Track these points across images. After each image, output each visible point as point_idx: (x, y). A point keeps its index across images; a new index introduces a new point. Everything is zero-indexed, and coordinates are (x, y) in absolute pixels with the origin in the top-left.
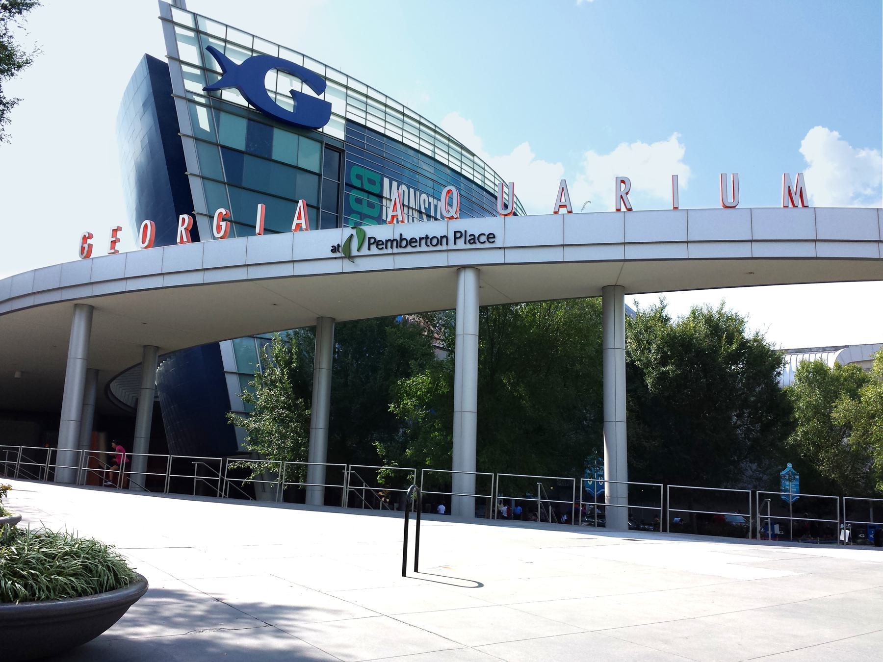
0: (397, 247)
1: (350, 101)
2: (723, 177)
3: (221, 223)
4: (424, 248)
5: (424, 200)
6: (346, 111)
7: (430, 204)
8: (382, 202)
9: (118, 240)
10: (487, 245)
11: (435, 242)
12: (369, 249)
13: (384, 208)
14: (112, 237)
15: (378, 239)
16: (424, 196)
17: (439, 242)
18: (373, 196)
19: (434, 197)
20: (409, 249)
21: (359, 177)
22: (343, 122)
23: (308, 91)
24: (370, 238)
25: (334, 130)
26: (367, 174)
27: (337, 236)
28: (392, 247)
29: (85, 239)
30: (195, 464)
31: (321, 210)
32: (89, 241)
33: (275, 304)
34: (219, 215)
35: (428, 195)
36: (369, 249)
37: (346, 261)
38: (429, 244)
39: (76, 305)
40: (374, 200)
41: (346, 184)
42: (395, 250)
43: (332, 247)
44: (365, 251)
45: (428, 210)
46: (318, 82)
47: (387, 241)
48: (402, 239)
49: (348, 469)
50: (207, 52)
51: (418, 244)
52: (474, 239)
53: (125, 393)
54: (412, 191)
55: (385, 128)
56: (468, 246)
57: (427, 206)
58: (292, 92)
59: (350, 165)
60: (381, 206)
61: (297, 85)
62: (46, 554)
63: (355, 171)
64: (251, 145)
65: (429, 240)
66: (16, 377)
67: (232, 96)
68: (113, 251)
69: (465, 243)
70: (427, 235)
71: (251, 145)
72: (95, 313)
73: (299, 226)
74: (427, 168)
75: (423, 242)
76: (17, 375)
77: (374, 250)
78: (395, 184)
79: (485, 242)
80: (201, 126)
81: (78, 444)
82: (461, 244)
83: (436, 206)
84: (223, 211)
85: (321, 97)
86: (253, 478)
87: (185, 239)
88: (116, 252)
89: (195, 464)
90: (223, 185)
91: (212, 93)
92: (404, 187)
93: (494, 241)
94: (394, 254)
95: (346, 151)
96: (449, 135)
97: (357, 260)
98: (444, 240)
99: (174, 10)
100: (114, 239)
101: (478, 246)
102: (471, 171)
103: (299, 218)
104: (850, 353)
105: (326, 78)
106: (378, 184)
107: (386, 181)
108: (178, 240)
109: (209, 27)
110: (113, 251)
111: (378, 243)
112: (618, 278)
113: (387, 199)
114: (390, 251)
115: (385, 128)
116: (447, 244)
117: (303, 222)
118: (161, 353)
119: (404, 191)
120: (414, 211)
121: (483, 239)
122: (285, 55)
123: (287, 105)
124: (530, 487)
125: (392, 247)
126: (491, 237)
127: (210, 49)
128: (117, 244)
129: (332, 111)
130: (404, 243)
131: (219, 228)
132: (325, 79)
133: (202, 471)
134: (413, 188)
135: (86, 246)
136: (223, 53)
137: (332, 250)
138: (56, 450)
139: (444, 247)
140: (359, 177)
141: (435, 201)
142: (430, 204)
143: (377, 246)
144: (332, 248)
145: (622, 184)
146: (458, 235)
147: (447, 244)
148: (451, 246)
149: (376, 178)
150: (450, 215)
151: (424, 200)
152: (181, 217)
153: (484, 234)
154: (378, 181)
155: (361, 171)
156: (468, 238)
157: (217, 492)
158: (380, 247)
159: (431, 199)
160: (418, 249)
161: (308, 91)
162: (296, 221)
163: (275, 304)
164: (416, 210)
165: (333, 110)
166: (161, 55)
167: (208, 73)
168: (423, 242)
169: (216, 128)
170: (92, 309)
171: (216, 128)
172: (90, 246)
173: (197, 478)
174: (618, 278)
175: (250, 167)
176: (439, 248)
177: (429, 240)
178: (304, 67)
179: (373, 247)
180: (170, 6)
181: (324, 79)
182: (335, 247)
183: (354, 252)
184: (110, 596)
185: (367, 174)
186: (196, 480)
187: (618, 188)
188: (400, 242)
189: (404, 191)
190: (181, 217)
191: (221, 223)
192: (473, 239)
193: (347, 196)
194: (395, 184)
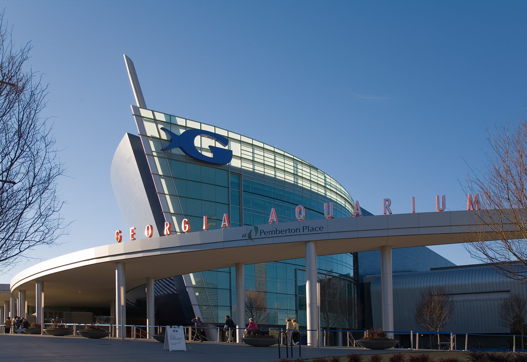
1: (243, 148)
2: (438, 197)
3: (186, 225)
4: (288, 234)
6: (241, 153)
10: (320, 232)
14: (132, 232)
23: (219, 145)
27: (245, 230)
29: (118, 234)
30: (131, 327)
31: (230, 205)
37: (250, 241)
38: (290, 232)
41: (243, 191)
42: (274, 235)
44: (258, 236)
52: (313, 229)
53: (132, 298)
55: (302, 174)
58: (210, 147)
65: (290, 230)
68: (133, 239)
69: (308, 231)
75: (288, 231)
77: (263, 235)
80: (175, 217)
82: (306, 231)
84: (187, 220)
85: (226, 148)
86: (197, 334)
88: (135, 239)
90: (165, 159)
95: (242, 174)
98: (298, 230)
99: (140, 109)
100: (133, 233)
101: (315, 232)
102: (316, 178)
103: (225, 221)
105: (228, 137)
110: (133, 239)
114: (271, 235)
115: (302, 174)
116: (299, 232)
121: (317, 229)
129: (233, 154)
130: (278, 232)
131: (185, 227)
135: (119, 236)
136: (170, 130)
138: (155, 326)
139: (298, 233)
145: (387, 202)
147: (299, 232)
153: (318, 227)
156: (310, 229)
160: (285, 234)
161: (219, 145)
165: (233, 154)
166: (137, 132)
168: (288, 231)
169: (170, 168)
171: (170, 168)
172: (121, 236)
176: (295, 233)
177: (290, 230)
178: (216, 133)
180: (139, 108)
181: (227, 138)
183: (253, 236)
184: (251, 339)
187: (385, 204)
191: (186, 225)
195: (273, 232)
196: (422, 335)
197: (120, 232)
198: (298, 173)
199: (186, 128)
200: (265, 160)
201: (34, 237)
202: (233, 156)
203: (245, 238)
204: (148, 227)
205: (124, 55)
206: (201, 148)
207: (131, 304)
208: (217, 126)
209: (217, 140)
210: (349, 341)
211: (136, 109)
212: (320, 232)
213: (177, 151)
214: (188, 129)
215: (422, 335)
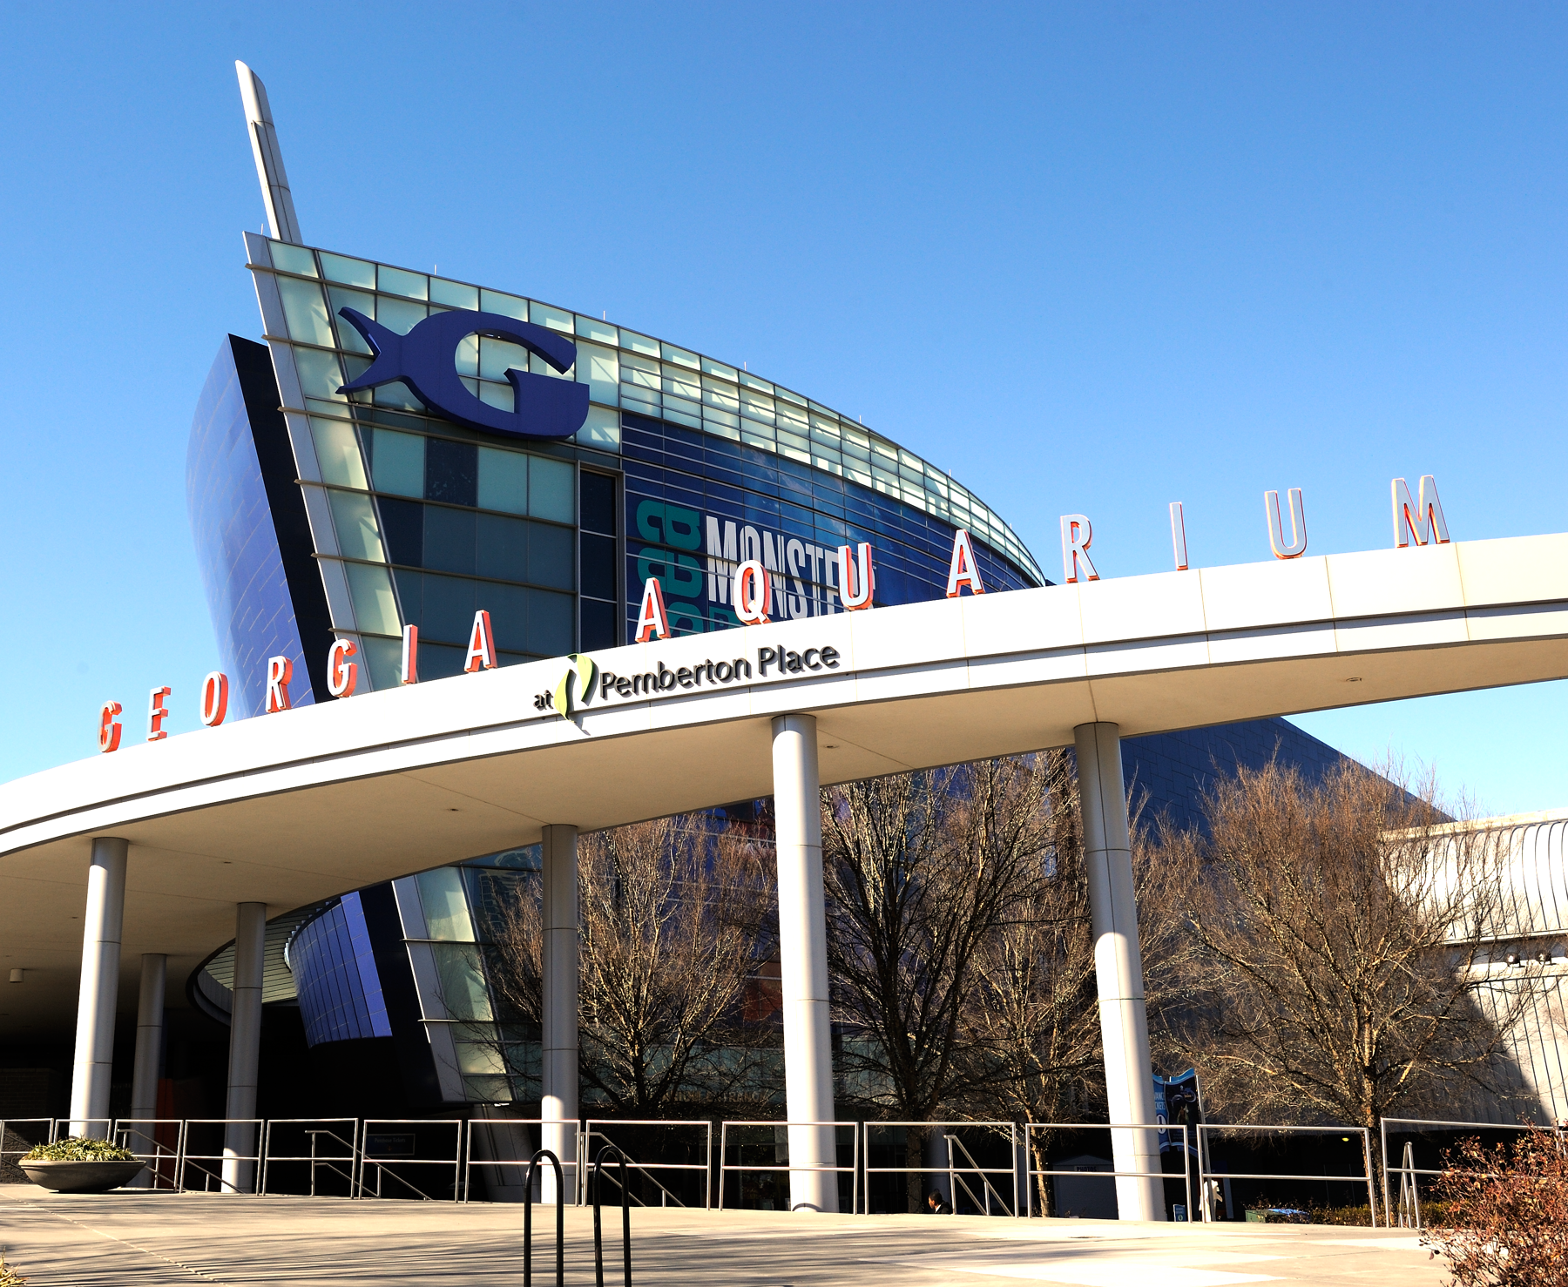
0: (655, 688)
4: (706, 685)
5: (796, 552)
7: (808, 558)
8: (705, 566)
9: (164, 713)
11: (724, 672)
12: (604, 695)
13: (711, 578)
15: (618, 676)
16: (794, 544)
17: (734, 672)
18: (685, 557)
19: (815, 544)
20: (679, 690)
21: (654, 521)
22: (615, 414)
24: (605, 675)
25: (604, 432)
26: (670, 515)
27: (548, 673)
28: (646, 689)
29: (107, 716)
32: (115, 719)
33: (453, 810)
34: (336, 653)
35: (804, 542)
36: (604, 695)
38: (714, 678)
39: (95, 840)
40: (687, 565)
42: (652, 694)
43: (537, 697)
45: (805, 573)
46: (560, 350)
47: (637, 678)
48: (663, 673)
49: (583, 1129)
50: (341, 320)
51: (631, 690)
54: (768, 536)
56: (789, 675)
57: (802, 563)
58: (509, 373)
59: (634, 502)
60: (705, 576)
61: (514, 358)
62: (1394, 1199)
63: (644, 511)
64: (435, 486)
65: (714, 671)
66: (12, 980)
67: (396, 394)
68: (155, 734)
70: (709, 661)
71: (435, 486)
72: (132, 854)
73: (477, 659)
74: (797, 488)
75: (703, 674)
76: (14, 976)
77: (614, 697)
78: (730, 527)
79: (817, 664)
81: (91, 1114)
83: (822, 562)
85: (569, 375)
87: (279, 704)
89: (311, 1134)
91: (356, 397)
92: (750, 531)
93: (835, 662)
94: (650, 703)
95: (625, 474)
96: (840, 415)
97: (588, 721)
98: (742, 668)
100: (156, 712)
104: (1497, 847)
106: (695, 531)
107: (712, 523)
108: (268, 706)
109: (336, 271)
110: (155, 734)
111: (619, 684)
112: (1095, 709)
113: (715, 558)
114: (642, 696)
117: (483, 652)
118: (271, 915)
119: (750, 538)
120: (775, 577)
122: (497, 306)
123: (500, 400)
124: (925, 1149)
125: (646, 689)
126: (828, 654)
127: (347, 314)
128: (163, 720)
130: (667, 681)
132: (575, 339)
133: (325, 1147)
134: (768, 530)
135: (109, 728)
137: (536, 703)
140: (654, 521)
141: (820, 550)
142: (808, 558)
143: (619, 689)
144: (536, 700)
146: (766, 657)
148: (757, 678)
149: (691, 520)
150: (750, 617)
151: (796, 552)
152: (271, 661)
154: (693, 523)
155: (657, 510)
157: (364, 1184)
158: (624, 691)
159: (810, 549)
160: (695, 689)
162: (471, 653)
163: (453, 810)
164: (778, 574)
165: (592, 397)
166: (256, 331)
167: (345, 357)
168: (703, 674)
170: (124, 843)
172: (117, 729)
173: (316, 1161)
174: (1095, 709)
175: (433, 524)
176: (734, 683)
177: (714, 671)
179: (611, 692)
181: (571, 341)
182: (542, 698)
185: (670, 515)
186: (316, 1167)
188: (660, 679)
189: (750, 538)
190: (271, 661)
192: (796, 663)
193: (633, 563)
194: (730, 527)
195: (650, 682)
196: (1346, 1140)
197: (118, 708)
198: (936, 501)
199: (431, 308)
200: (809, 455)
201: (1533, 913)
202: (590, 407)
203: (547, 712)
204: (212, 681)
205: (242, 71)
206: (479, 378)
207: (501, 1031)
208: (536, 298)
209: (532, 348)
210: (990, 1192)
211: (262, 243)
212: (825, 670)
213: (396, 394)
214: (434, 311)
215: (1346, 1140)
